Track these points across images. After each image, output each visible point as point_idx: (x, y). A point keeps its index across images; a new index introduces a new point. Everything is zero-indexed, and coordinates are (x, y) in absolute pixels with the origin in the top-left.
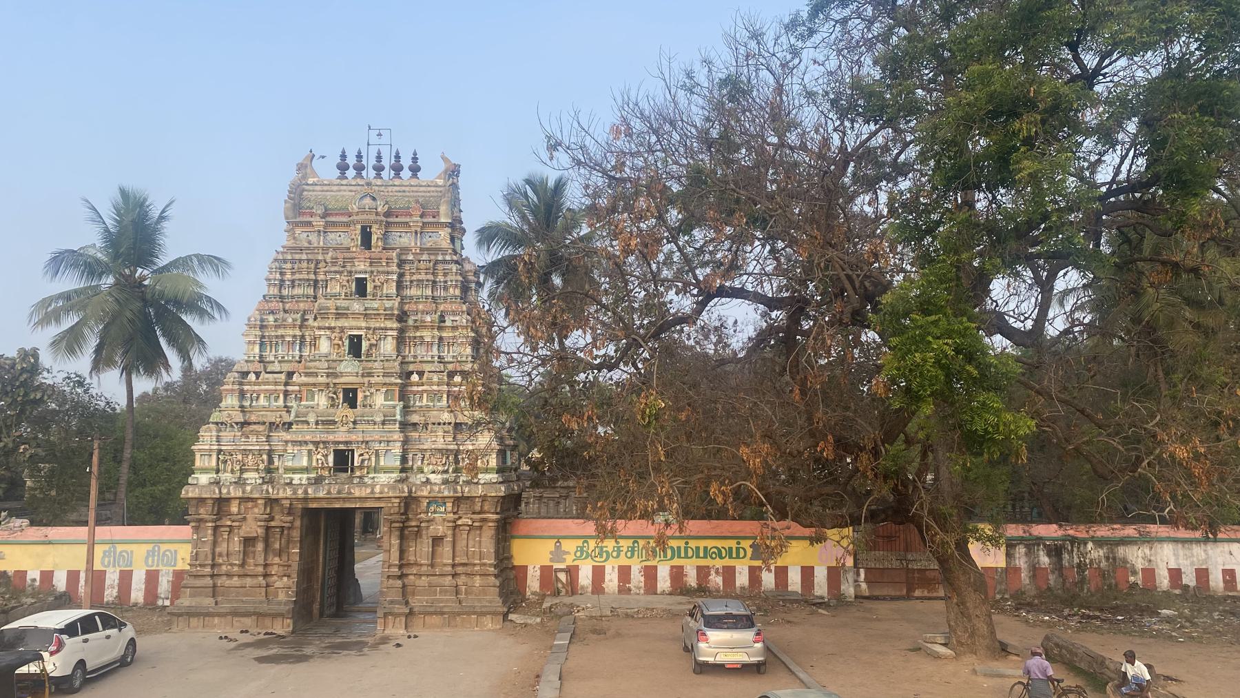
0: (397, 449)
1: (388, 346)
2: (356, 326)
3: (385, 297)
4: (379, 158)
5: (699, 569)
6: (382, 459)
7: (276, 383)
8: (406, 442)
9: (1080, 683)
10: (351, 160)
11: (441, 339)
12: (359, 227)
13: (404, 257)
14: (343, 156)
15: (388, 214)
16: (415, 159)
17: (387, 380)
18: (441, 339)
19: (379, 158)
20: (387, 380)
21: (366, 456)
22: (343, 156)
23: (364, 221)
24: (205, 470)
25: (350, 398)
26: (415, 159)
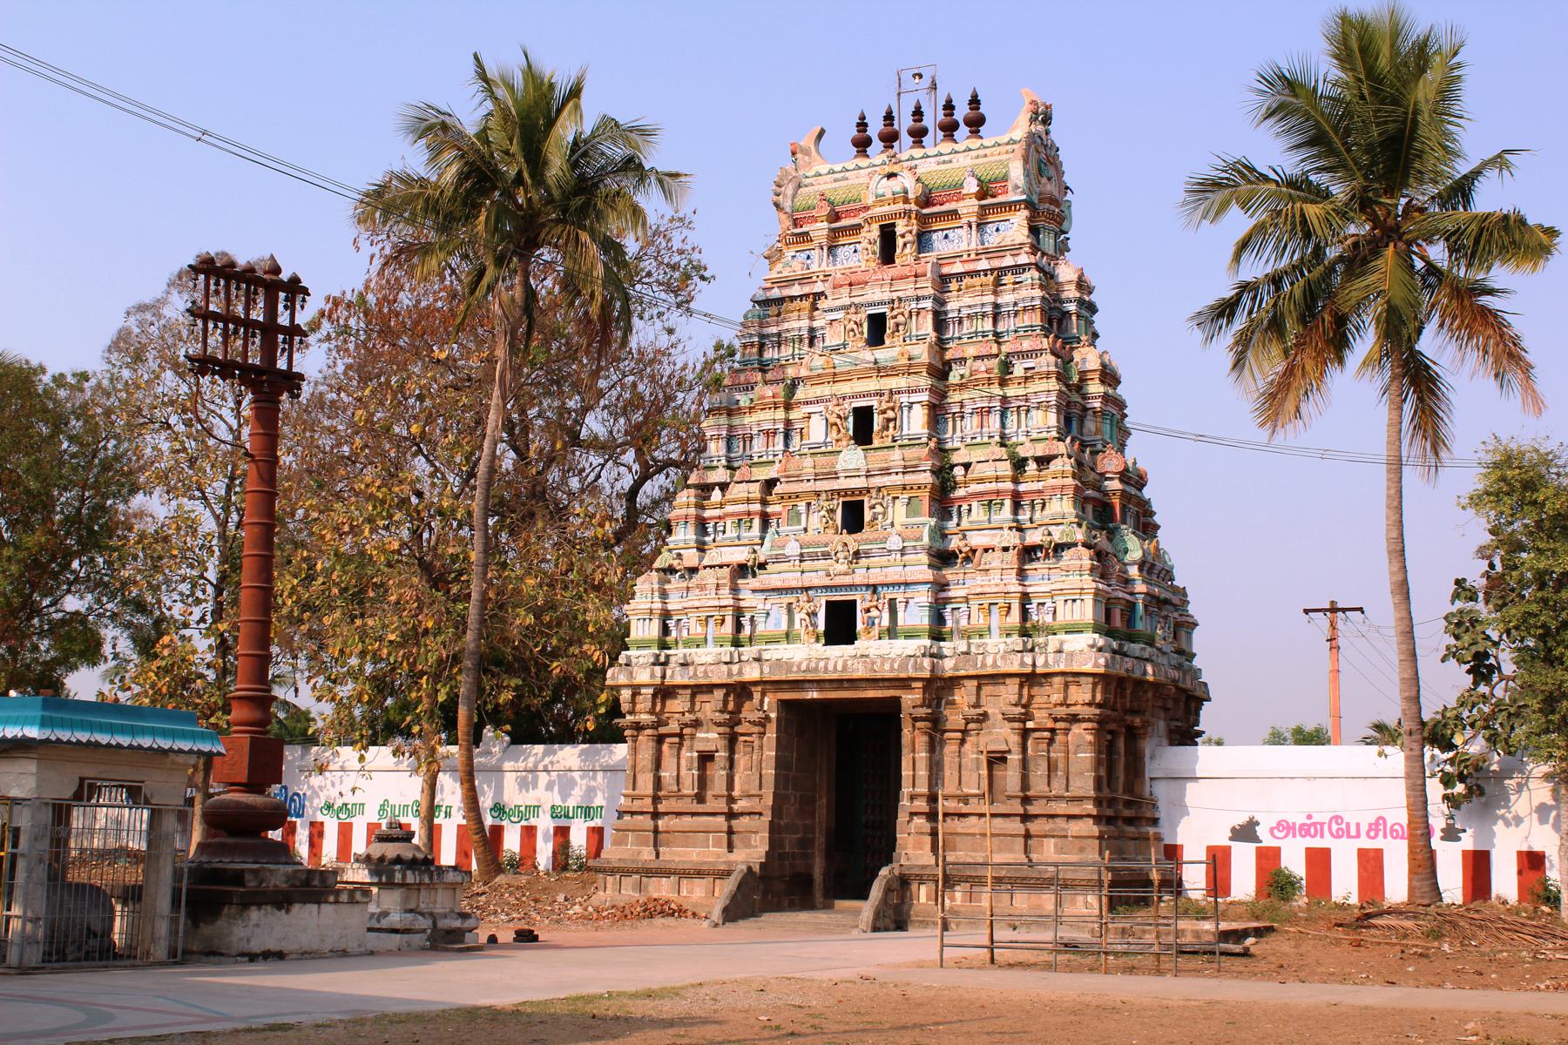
0: (923, 596)
1: (916, 422)
2: (861, 390)
3: (912, 343)
4: (918, 113)
5: (1363, 854)
6: (900, 615)
7: (748, 501)
8: (940, 586)
9: (773, 715)
10: (875, 128)
11: (1004, 399)
12: (875, 227)
13: (945, 270)
14: (862, 125)
15: (926, 200)
16: (975, 102)
17: (910, 478)
18: (1004, 399)
19: (918, 113)
20: (910, 478)
21: (874, 613)
22: (862, 125)
23: (883, 217)
24: (643, 645)
25: (853, 518)
26: (975, 102)
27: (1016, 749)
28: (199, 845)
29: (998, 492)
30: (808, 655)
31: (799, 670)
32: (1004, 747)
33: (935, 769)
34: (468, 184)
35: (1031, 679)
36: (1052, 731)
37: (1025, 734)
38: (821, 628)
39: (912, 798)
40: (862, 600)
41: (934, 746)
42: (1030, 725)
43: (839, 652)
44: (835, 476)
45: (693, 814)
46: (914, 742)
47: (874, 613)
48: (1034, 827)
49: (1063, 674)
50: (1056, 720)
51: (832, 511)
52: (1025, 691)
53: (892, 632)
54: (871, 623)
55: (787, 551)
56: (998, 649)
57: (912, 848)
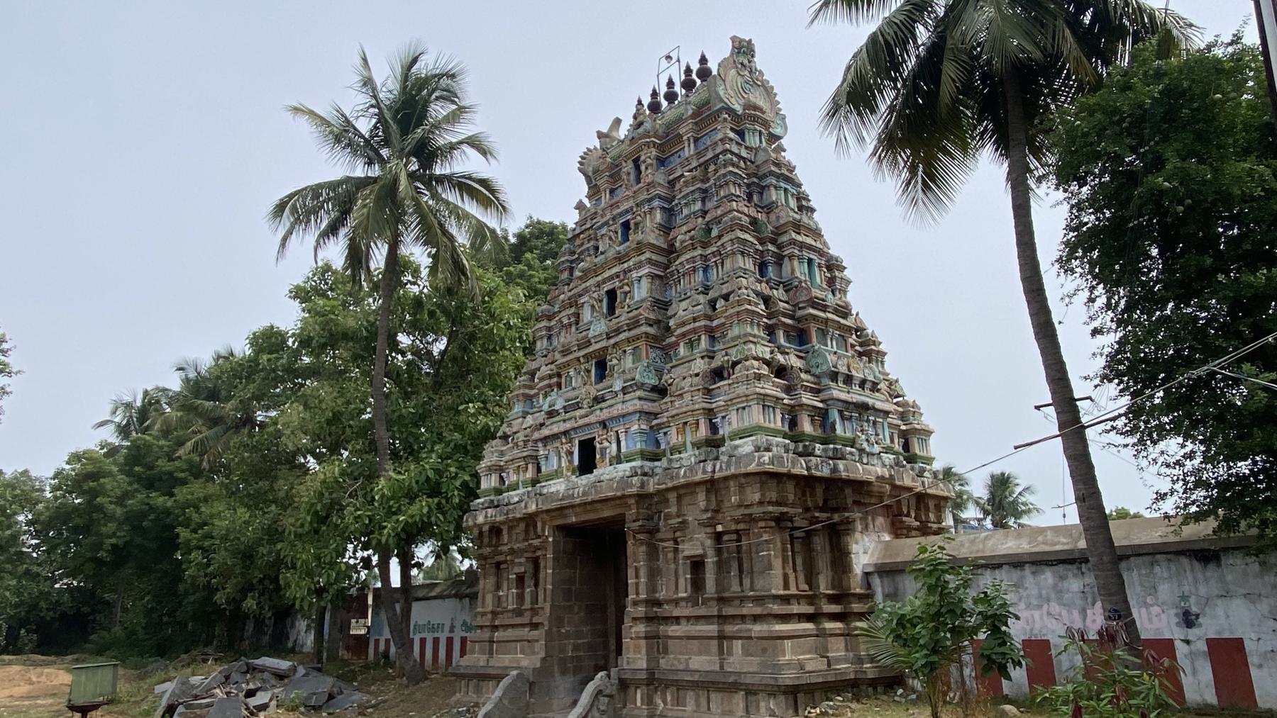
11: (705, 258)
27: (711, 552)
28: (1121, 368)
29: (694, 331)
30: (563, 485)
31: (611, 487)
32: (700, 552)
33: (654, 574)
34: (789, 321)
35: (712, 485)
36: (737, 532)
37: (718, 537)
38: (576, 462)
39: (635, 603)
40: (597, 432)
41: (653, 553)
42: (720, 528)
43: (585, 479)
44: (589, 343)
45: (513, 626)
46: (636, 555)
47: (606, 444)
48: (730, 629)
49: (735, 476)
50: (738, 522)
51: (589, 371)
52: (713, 498)
53: (618, 459)
54: (603, 455)
55: (557, 407)
56: (688, 463)
57: (635, 658)
